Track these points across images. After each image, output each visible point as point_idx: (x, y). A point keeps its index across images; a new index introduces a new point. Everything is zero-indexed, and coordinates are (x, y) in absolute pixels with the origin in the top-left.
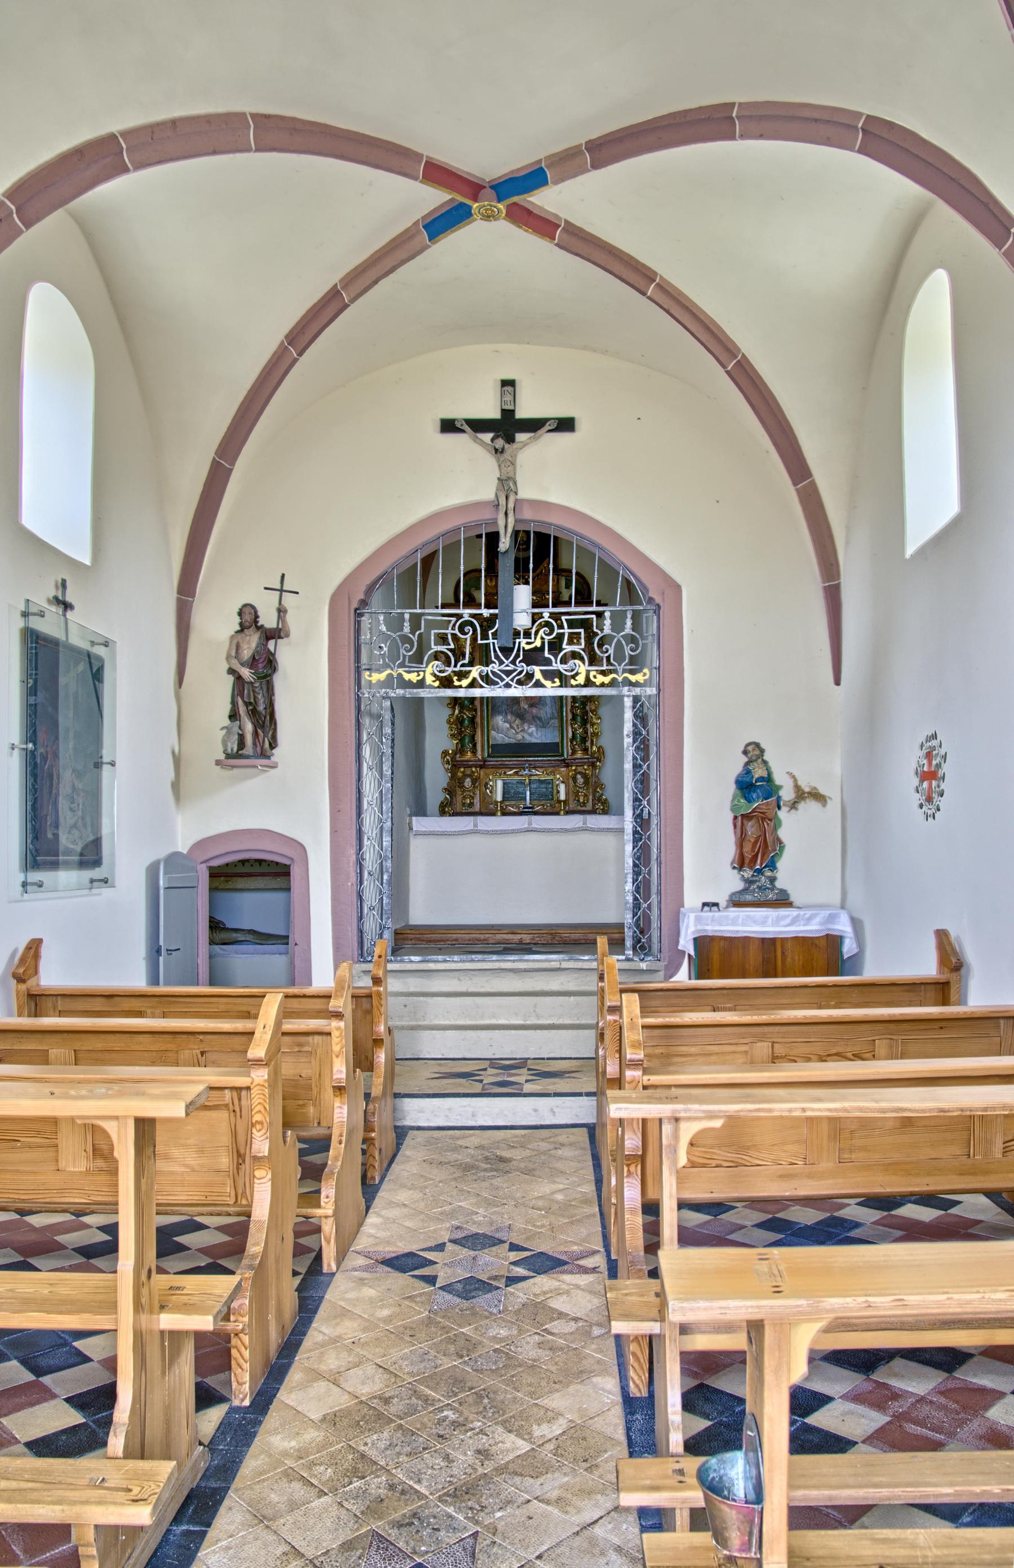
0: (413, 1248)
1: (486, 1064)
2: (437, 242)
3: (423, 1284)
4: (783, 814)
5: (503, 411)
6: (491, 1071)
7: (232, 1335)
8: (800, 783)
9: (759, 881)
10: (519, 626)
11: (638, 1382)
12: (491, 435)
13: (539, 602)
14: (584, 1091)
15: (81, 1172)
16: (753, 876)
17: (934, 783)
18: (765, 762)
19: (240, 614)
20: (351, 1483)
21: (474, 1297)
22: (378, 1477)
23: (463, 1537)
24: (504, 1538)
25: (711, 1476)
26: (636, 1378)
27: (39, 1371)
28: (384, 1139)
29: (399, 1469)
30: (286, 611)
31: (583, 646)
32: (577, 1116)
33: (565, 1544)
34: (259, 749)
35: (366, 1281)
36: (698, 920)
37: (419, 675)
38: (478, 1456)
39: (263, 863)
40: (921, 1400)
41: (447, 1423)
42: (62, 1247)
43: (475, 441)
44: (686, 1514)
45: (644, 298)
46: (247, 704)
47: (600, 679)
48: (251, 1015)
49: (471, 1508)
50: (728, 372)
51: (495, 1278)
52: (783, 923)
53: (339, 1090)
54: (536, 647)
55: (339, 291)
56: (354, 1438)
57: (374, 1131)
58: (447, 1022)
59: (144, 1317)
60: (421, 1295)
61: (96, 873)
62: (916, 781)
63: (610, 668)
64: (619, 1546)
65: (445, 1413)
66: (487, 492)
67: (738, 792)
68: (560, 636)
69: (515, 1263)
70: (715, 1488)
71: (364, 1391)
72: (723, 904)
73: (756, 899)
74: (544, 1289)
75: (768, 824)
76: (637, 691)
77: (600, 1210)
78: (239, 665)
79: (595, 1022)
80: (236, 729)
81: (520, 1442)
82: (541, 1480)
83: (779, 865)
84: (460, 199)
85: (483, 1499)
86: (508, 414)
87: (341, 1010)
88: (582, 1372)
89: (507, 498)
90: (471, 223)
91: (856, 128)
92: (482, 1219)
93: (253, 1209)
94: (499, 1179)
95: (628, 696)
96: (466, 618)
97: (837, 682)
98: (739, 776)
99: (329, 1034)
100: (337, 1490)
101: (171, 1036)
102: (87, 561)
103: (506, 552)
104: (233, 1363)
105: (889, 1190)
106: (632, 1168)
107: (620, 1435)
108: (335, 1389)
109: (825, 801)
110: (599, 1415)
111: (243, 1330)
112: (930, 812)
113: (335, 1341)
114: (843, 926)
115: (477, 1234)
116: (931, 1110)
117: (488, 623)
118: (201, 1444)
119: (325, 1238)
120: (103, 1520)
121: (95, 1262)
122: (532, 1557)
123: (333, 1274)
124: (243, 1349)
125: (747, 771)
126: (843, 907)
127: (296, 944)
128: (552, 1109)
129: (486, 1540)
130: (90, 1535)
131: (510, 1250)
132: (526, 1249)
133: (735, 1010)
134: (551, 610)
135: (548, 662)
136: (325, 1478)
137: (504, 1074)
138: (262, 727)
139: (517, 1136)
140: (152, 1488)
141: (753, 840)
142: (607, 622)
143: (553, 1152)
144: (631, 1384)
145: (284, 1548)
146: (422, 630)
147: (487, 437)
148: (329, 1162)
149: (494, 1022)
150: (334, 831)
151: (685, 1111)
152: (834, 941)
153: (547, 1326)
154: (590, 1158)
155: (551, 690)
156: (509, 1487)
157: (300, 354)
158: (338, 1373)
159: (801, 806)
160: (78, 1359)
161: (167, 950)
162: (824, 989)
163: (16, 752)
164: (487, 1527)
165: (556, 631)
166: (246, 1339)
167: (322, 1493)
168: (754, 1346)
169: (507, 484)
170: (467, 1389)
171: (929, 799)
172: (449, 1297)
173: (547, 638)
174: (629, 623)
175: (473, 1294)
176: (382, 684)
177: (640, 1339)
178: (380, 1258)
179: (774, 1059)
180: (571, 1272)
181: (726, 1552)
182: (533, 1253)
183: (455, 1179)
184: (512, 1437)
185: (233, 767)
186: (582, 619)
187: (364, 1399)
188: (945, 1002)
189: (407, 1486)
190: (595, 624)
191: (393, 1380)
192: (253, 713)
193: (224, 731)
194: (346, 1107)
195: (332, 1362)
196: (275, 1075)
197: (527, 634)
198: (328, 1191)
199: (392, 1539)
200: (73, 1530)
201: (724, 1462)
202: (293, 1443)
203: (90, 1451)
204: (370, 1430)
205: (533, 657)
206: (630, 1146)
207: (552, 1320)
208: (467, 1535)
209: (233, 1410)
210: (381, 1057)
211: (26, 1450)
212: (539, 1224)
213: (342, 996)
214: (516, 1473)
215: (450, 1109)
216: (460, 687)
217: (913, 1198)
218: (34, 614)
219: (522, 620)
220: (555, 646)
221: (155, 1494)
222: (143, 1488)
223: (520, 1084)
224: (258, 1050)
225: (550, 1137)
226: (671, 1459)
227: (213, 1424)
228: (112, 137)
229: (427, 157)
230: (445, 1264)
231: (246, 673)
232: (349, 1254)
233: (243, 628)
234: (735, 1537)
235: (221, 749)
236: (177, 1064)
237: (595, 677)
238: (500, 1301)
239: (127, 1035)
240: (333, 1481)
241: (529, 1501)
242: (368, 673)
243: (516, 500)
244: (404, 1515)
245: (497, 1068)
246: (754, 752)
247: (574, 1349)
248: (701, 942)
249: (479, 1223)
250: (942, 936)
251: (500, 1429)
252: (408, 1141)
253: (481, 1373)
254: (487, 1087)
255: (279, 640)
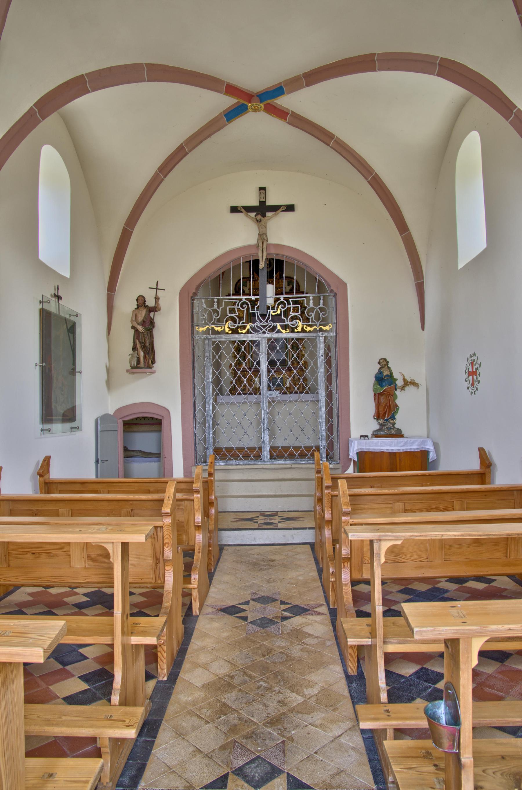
0: (234, 603)
1: (258, 514)
2: (231, 122)
3: (241, 621)
4: (398, 392)
5: (260, 202)
6: (261, 517)
7: (158, 646)
8: (405, 378)
9: (387, 425)
10: (269, 304)
11: (352, 667)
12: (255, 214)
13: (278, 291)
14: (307, 527)
15: (82, 568)
16: (384, 422)
17: (475, 377)
18: (389, 368)
19: (137, 300)
20: (220, 717)
21: (267, 627)
22: (233, 714)
23: (278, 743)
24: (297, 744)
25: (429, 713)
26: (351, 666)
27: (64, 664)
28: (215, 551)
29: (242, 711)
30: (159, 299)
31: (300, 313)
32: (304, 539)
33: (327, 746)
34: (146, 364)
35: (214, 620)
36: (359, 444)
37: (222, 328)
38: (280, 704)
39: (146, 419)
40: (490, 676)
41: (262, 688)
42: (66, 604)
43: (247, 217)
44: (392, 731)
45: (329, 147)
46: (141, 343)
47: (308, 329)
48: (164, 491)
49: (280, 729)
50: (368, 182)
51: (276, 617)
52: (400, 445)
53: (198, 527)
54: (278, 314)
55: (183, 147)
56: (219, 695)
57: (211, 547)
58: (238, 494)
59: (125, 638)
60: (241, 626)
61: (74, 424)
62: (465, 376)
63: (313, 323)
64: (354, 747)
65: (261, 683)
66: (253, 240)
67: (376, 382)
68: (289, 309)
69: (284, 610)
70: (432, 718)
71: (220, 673)
72: (370, 436)
73: (386, 434)
74: (300, 623)
75: (391, 398)
76: (326, 334)
77: (322, 585)
78: (137, 325)
79: (313, 493)
80: (136, 355)
81: (298, 697)
82: (311, 716)
83: (396, 417)
84: (243, 102)
85: (285, 725)
86: (262, 203)
87: (198, 489)
88: (324, 663)
89: (263, 243)
90: (247, 113)
91: (436, 64)
92: (265, 589)
93: (165, 585)
94: (271, 570)
95: (322, 337)
96: (244, 300)
97: (423, 329)
98: (376, 374)
99: (193, 500)
100: (214, 721)
101: (107, 502)
102: (68, 276)
103: (263, 269)
104: (159, 659)
105: (468, 574)
106: (346, 564)
107: (346, 693)
108: (207, 672)
109: (418, 386)
110: (335, 684)
111: (163, 643)
112: (473, 391)
113: (203, 648)
114: (429, 446)
115: (264, 596)
116: (503, 535)
117: (254, 303)
118: (147, 699)
119: (194, 599)
120: (113, 736)
121: (84, 611)
122: (312, 753)
123: (198, 616)
124: (163, 653)
125: (380, 372)
126: (428, 437)
127: (165, 457)
128: (292, 536)
129: (289, 744)
130: (107, 742)
131: (281, 604)
132: (288, 604)
133: (381, 487)
134: (284, 296)
135: (284, 321)
136: (208, 715)
137: (267, 519)
138: (148, 353)
139: (276, 549)
140: (135, 720)
141: (384, 405)
142: (311, 302)
143: (295, 556)
144: (349, 668)
145: (192, 749)
146: (223, 307)
147: (253, 214)
148: (194, 562)
149: (260, 493)
150: (183, 403)
151: (385, 536)
152: (425, 453)
153: (303, 641)
154: (313, 560)
155: (285, 334)
156: (296, 719)
157: (165, 177)
158: (207, 664)
159: (407, 388)
160: (82, 658)
161: (102, 461)
162: (424, 477)
163: (38, 367)
164: (289, 738)
165: (287, 306)
166: (165, 648)
167: (207, 722)
168: (450, 649)
169: (262, 236)
170: (269, 671)
171: (473, 385)
172: (254, 627)
173: (283, 309)
174: (322, 302)
175: (266, 625)
176: (204, 332)
177: (353, 647)
178: (219, 608)
179: (405, 511)
180: (312, 615)
181: (441, 749)
182: (292, 605)
183: (250, 570)
184: (294, 694)
185: (134, 373)
186: (296, 301)
187: (221, 676)
188: (483, 483)
189: (247, 719)
190: (305, 302)
191: (234, 667)
192: (144, 347)
193: (130, 356)
194: (201, 535)
195: (203, 658)
196: (174, 520)
197: (273, 308)
198: (195, 576)
199: (244, 744)
200: (98, 740)
201: (435, 706)
202: (190, 698)
203: (94, 702)
204: (226, 691)
205: (277, 318)
206: (345, 553)
207: (306, 638)
208: (279, 742)
209: (159, 682)
210: (213, 511)
211: (63, 701)
212: (293, 591)
213: (199, 482)
214: (299, 712)
215: (243, 536)
216: (242, 333)
217: (472, 578)
218: (45, 302)
219: (270, 301)
220: (286, 313)
221: (137, 723)
222: (131, 720)
223: (276, 523)
224: (166, 509)
225: (293, 549)
226: (382, 705)
227: (151, 689)
228: (82, 76)
229: (227, 82)
230: (251, 611)
231: (140, 328)
232: (204, 606)
233: (138, 306)
234: (446, 742)
235: (129, 365)
236: (120, 516)
237: (306, 328)
238: (279, 629)
239: (96, 502)
240: (211, 716)
241: (307, 726)
242: (197, 327)
243: (267, 244)
244: (248, 733)
245: (264, 516)
246: (384, 363)
247: (318, 652)
248: (360, 454)
249: (265, 591)
250: (482, 452)
251: (288, 691)
252: (224, 552)
253: (276, 664)
254: (260, 525)
255: (156, 313)
